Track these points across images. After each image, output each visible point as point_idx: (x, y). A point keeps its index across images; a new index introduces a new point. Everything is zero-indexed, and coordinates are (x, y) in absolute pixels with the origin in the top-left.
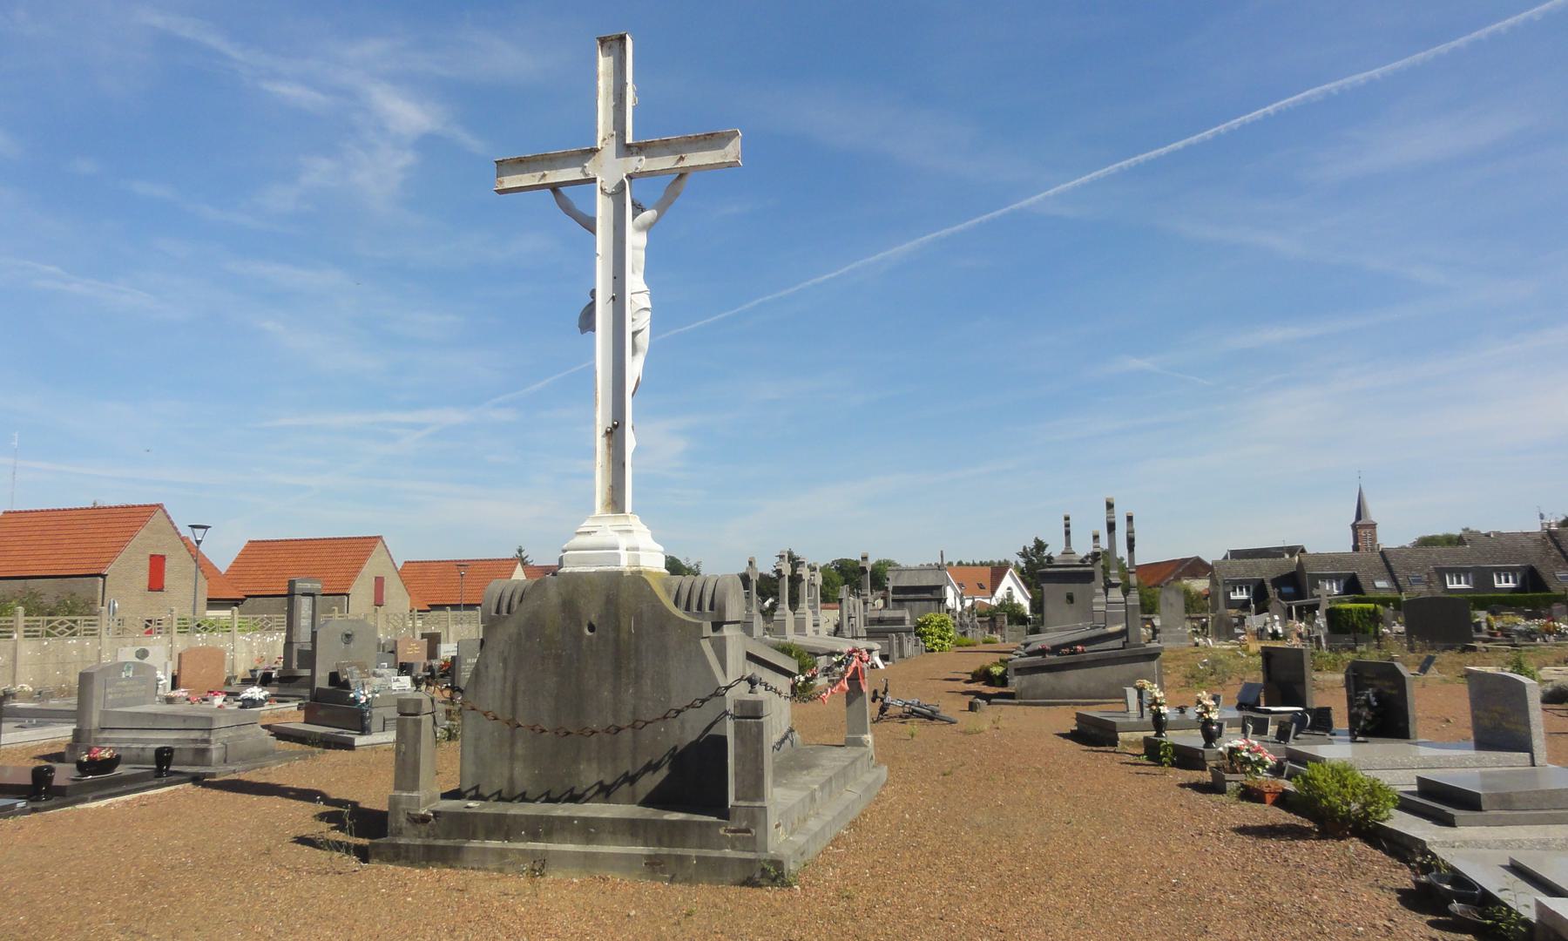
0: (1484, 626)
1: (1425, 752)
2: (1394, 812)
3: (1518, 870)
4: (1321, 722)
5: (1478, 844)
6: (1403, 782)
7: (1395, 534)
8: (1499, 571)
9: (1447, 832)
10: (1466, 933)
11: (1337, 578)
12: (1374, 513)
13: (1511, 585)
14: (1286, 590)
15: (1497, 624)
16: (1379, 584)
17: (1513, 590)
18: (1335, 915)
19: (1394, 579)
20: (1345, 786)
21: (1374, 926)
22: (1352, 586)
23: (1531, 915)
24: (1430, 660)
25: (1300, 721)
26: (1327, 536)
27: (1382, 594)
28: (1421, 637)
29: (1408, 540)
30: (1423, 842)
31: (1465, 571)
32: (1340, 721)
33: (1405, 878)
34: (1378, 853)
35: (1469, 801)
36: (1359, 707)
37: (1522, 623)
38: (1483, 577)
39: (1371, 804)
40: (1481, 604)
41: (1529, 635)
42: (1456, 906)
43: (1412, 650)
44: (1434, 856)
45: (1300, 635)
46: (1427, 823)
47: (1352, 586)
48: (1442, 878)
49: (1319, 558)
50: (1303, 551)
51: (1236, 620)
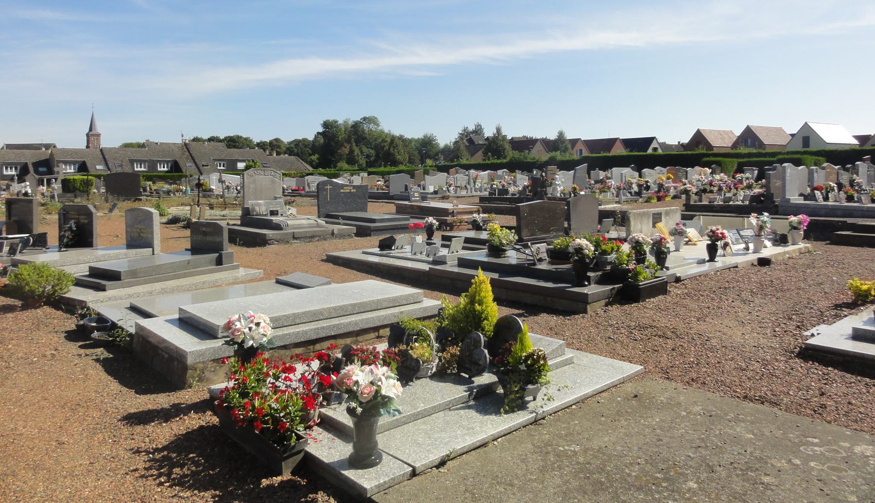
0: (148, 189)
1: (100, 253)
2: (72, 288)
3: (134, 309)
4: (41, 242)
5: (115, 298)
6: (81, 270)
7: (110, 140)
8: (160, 162)
9: (101, 294)
10: (99, 347)
11: (74, 163)
12: (99, 128)
13: (166, 169)
14: (41, 169)
15: (154, 188)
16: (98, 167)
17: (167, 172)
18: (20, 355)
19: (107, 165)
20: (42, 276)
21: (45, 356)
22: (83, 168)
23: (132, 330)
24: (114, 206)
25: (25, 243)
26: (69, 138)
27: (99, 173)
28: (112, 193)
29: (116, 144)
30: (85, 302)
31: (145, 161)
32: (53, 238)
33: (71, 323)
34: (60, 313)
35: (113, 276)
36: (65, 231)
37: (166, 187)
38: (152, 165)
39: (58, 285)
40: (149, 178)
41: (168, 192)
42: (96, 334)
43: (107, 201)
44: (88, 309)
45: (43, 194)
46: (91, 291)
47: (83, 168)
48: (91, 321)
49: (64, 151)
50: (55, 147)
51: (4, 187)
